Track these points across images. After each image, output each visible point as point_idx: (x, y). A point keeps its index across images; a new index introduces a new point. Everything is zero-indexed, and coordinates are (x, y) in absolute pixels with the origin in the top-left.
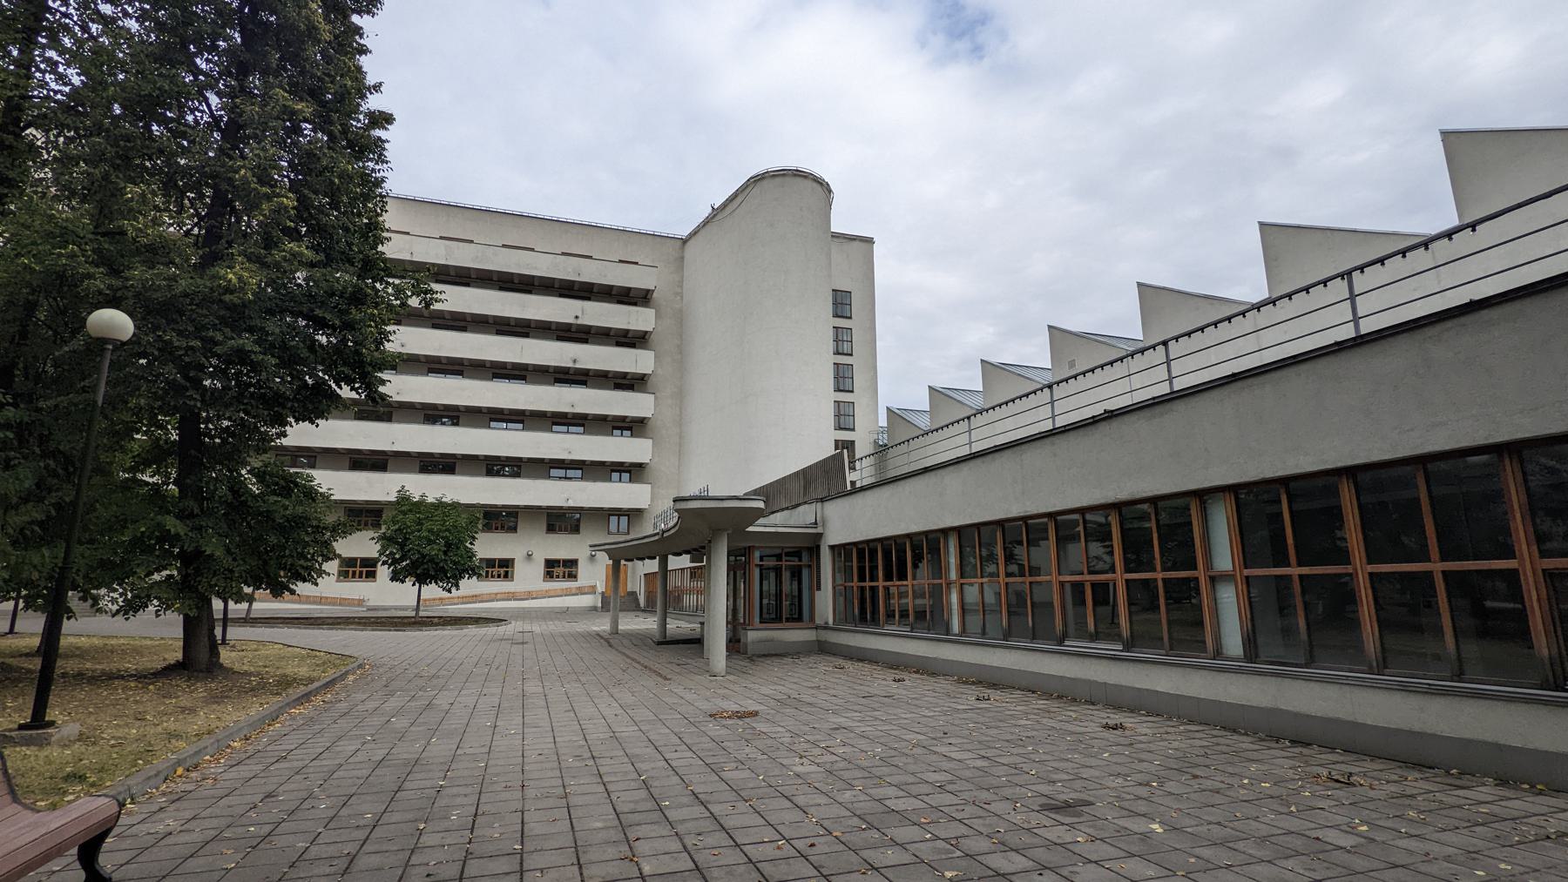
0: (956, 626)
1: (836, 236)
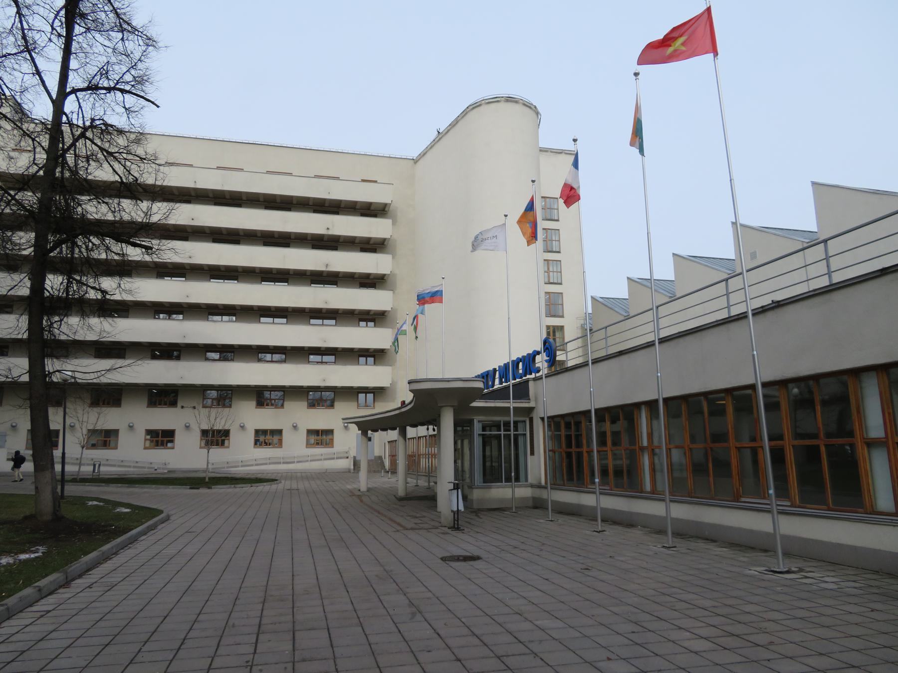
0: (648, 487)
1: (542, 150)
